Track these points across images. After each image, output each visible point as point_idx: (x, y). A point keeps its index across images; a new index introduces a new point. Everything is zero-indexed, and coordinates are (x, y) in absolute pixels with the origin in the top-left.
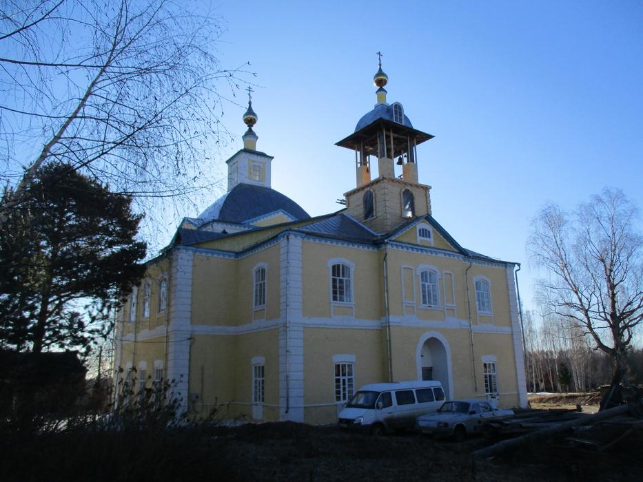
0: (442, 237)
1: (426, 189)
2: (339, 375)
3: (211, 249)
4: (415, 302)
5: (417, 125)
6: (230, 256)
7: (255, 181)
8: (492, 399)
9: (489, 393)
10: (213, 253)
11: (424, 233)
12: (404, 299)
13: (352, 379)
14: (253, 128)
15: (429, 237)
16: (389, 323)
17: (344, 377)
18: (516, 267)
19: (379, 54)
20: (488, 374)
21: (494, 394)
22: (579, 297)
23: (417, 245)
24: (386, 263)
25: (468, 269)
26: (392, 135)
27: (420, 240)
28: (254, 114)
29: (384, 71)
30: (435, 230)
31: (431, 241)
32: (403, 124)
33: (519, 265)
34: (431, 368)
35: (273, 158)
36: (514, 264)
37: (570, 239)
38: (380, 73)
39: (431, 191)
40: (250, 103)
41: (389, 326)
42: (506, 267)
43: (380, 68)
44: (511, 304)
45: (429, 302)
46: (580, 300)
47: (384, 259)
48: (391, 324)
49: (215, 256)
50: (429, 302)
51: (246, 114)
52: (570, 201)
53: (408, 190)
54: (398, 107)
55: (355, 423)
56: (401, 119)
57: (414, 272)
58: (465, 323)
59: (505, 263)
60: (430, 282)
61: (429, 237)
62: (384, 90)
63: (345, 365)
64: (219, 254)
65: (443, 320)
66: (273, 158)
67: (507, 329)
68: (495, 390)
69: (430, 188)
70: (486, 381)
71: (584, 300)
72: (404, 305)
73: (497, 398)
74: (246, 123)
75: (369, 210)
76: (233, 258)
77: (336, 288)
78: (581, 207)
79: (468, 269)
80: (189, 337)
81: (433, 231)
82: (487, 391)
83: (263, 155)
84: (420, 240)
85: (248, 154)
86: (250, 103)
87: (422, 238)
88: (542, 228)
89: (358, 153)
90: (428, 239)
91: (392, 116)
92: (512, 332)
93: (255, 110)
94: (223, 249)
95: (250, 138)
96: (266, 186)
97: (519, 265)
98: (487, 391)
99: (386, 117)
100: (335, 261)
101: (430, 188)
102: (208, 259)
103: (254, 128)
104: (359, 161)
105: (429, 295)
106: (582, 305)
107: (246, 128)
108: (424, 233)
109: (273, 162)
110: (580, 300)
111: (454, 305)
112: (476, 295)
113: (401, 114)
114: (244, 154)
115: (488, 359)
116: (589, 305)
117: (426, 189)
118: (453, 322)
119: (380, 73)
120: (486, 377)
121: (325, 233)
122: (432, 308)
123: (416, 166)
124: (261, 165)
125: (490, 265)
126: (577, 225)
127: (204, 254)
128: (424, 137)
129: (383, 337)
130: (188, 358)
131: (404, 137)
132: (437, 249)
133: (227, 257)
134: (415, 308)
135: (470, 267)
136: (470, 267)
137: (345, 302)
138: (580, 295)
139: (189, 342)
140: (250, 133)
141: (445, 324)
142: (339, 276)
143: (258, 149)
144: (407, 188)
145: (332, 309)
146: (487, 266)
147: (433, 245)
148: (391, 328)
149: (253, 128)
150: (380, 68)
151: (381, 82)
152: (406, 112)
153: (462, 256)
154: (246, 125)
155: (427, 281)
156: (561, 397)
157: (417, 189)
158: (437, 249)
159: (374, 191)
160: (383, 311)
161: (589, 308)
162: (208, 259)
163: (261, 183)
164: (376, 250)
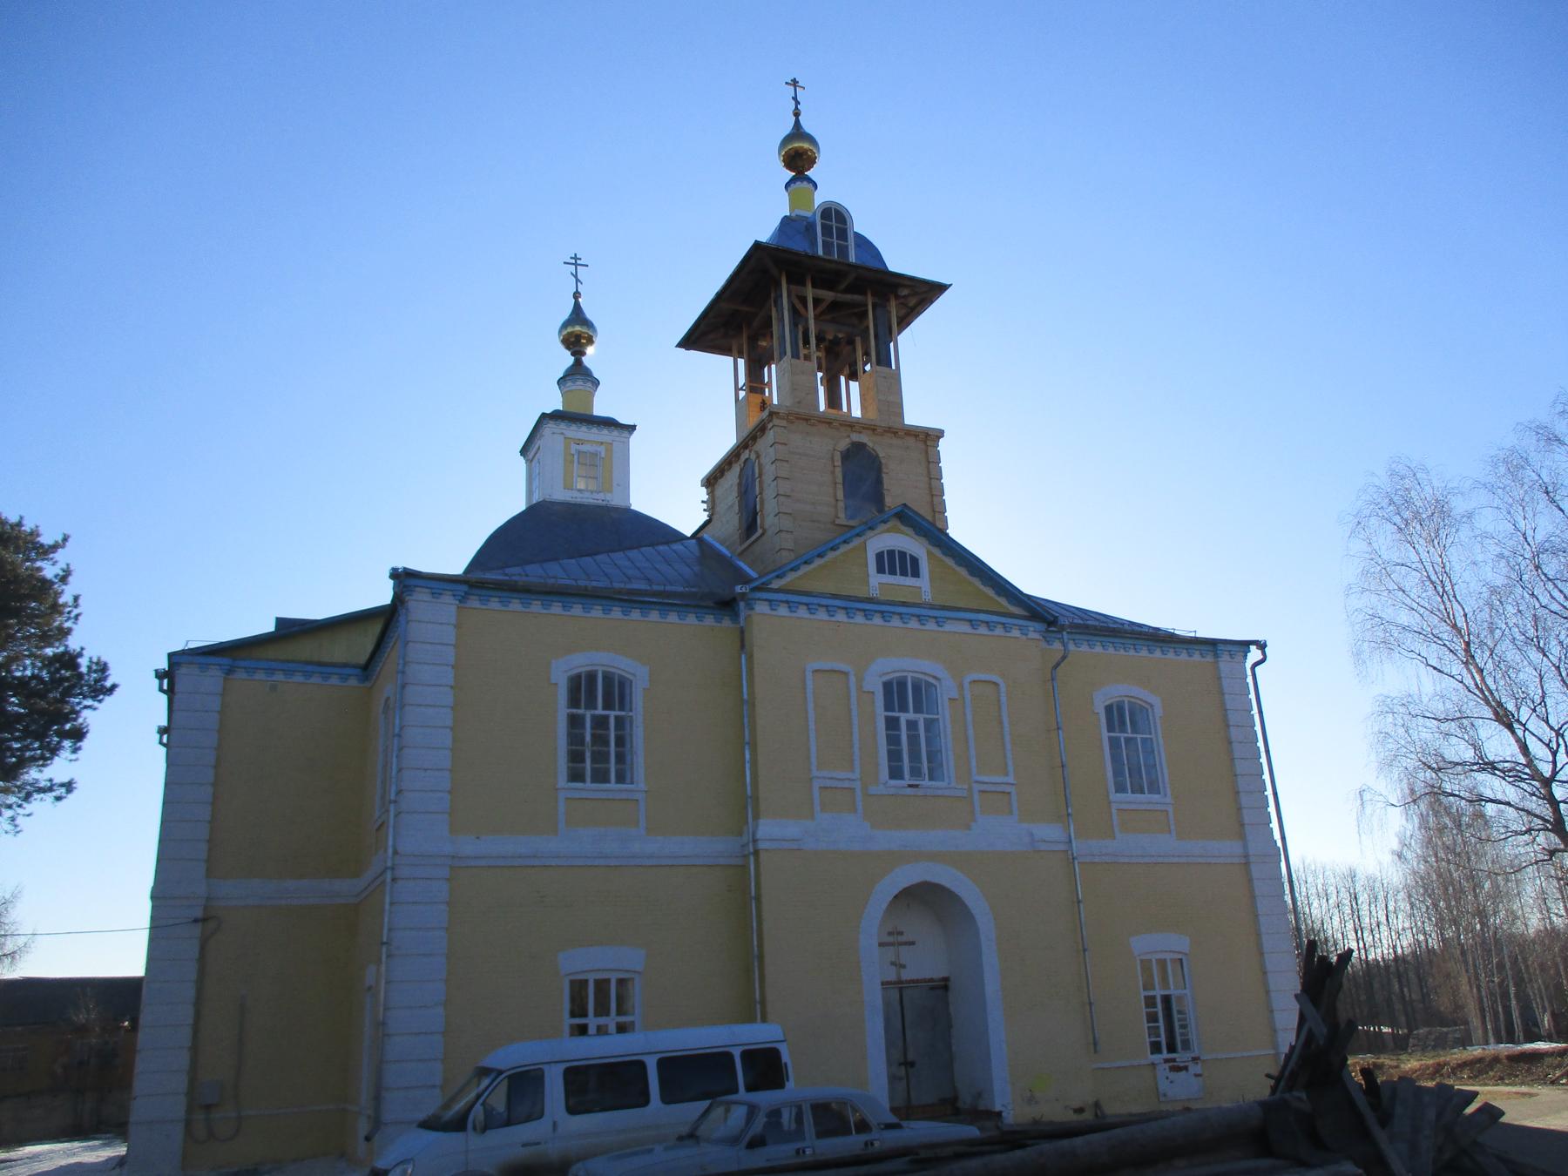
0: (963, 572)
1: (929, 437)
2: (585, 1015)
3: (283, 661)
4: (857, 775)
5: (897, 261)
6: (344, 678)
7: (582, 491)
8: (1173, 1075)
9: (1165, 1055)
10: (289, 673)
11: (894, 562)
12: (814, 768)
13: (573, 1015)
14: (570, 360)
15: (916, 574)
16: (755, 841)
17: (602, 1020)
18: (1254, 654)
19: (795, 83)
20: (1158, 993)
21: (1181, 1057)
22: (1518, 740)
23: (870, 600)
24: (750, 658)
25: (1058, 665)
26: (810, 293)
27: (877, 582)
28: (587, 323)
29: (808, 125)
30: (937, 552)
31: (923, 586)
32: (852, 259)
33: (1262, 646)
34: (946, 979)
35: (633, 428)
36: (1245, 645)
37: (1476, 571)
38: (798, 132)
39: (943, 445)
40: (577, 295)
41: (756, 853)
42: (1216, 656)
43: (797, 123)
44: (1241, 767)
45: (916, 772)
46: (1524, 749)
47: (743, 646)
48: (761, 845)
49: (298, 678)
50: (916, 772)
51: (566, 324)
52: (1456, 462)
53: (864, 445)
54: (835, 217)
55: (1503, 1120)
56: (843, 250)
57: (853, 679)
58: (1050, 832)
59: (1213, 644)
60: (918, 710)
61: (916, 574)
62: (809, 180)
63: (607, 981)
64: (307, 674)
65: (968, 827)
66: (633, 428)
67: (1228, 848)
68: (1187, 1045)
69: (939, 434)
70: (1152, 1018)
71: (1536, 748)
72: (816, 785)
73: (1194, 1069)
74: (568, 348)
75: (750, 524)
76: (353, 682)
77: (582, 742)
78: (1495, 466)
79: (1058, 665)
80: (199, 913)
81: (929, 553)
82: (1156, 1048)
83: (609, 423)
84: (877, 582)
85: (563, 425)
86: (577, 295)
87: (887, 578)
88: (1386, 541)
89: (741, 362)
90: (909, 581)
91: (814, 243)
92: (1246, 856)
93: (589, 313)
94: (326, 659)
95: (579, 385)
96: (615, 500)
97: (1262, 646)
98: (1156, 1048)
99: (799, 245)
100: (580, 662)
101: (939, 434)
102: (274, 688)
103: (568, 360)
104: (742, 380)
105: (913, 740)
106: (1530, 763)
107: (568, 360)
108: (894, 562)
109: (634, 439)
110: (1524, 749)
111: (1011, 779)
112: (881, 725)
113: (843, 234)
114: (550, 428)
115: (1146, 944)
116: (1554, 763)
117: (929, 437)
118: (1000, 832)
119: (798, 132)
120: (1150, 1002)
121: (568, 582)
122: (920, 792)
123: (896, 378)
124: (602, 449)
125: (1158, 653)
126: (1489, 521)
127: (260, 676)
128: (923, 293)
129: (742, 886)
130: (194, 977)
131: (857, 298)
132: (943, 608)
133: (334, 680)
134: (859, 793)
135: (1064, 658)
136: (1064, 658)
137: (613, 785)
138: (1520, 733)
139: (197, 930)
140: (578, 374)
141: (982, 834)
142: (591, 704)
143: (600, 409)
144: (856, 437)
145: (562, 808)
146: (1144, 654)
147: (927, 596)
148: (763, 856)
149: (570, 360)
150: (797, 123)
151: (798, 158)
152: (862, 224)
153: (1041, 626)
154: (569, 353)
155: (904, 709)
156: (1496, 1059)
157: (895, 441)
158: (943, 608)
159: (758, 457)
160: (744, 807)
161: (1555, 773)
162: (274, 688)
163: (601, 496)
164: (727, 622)
